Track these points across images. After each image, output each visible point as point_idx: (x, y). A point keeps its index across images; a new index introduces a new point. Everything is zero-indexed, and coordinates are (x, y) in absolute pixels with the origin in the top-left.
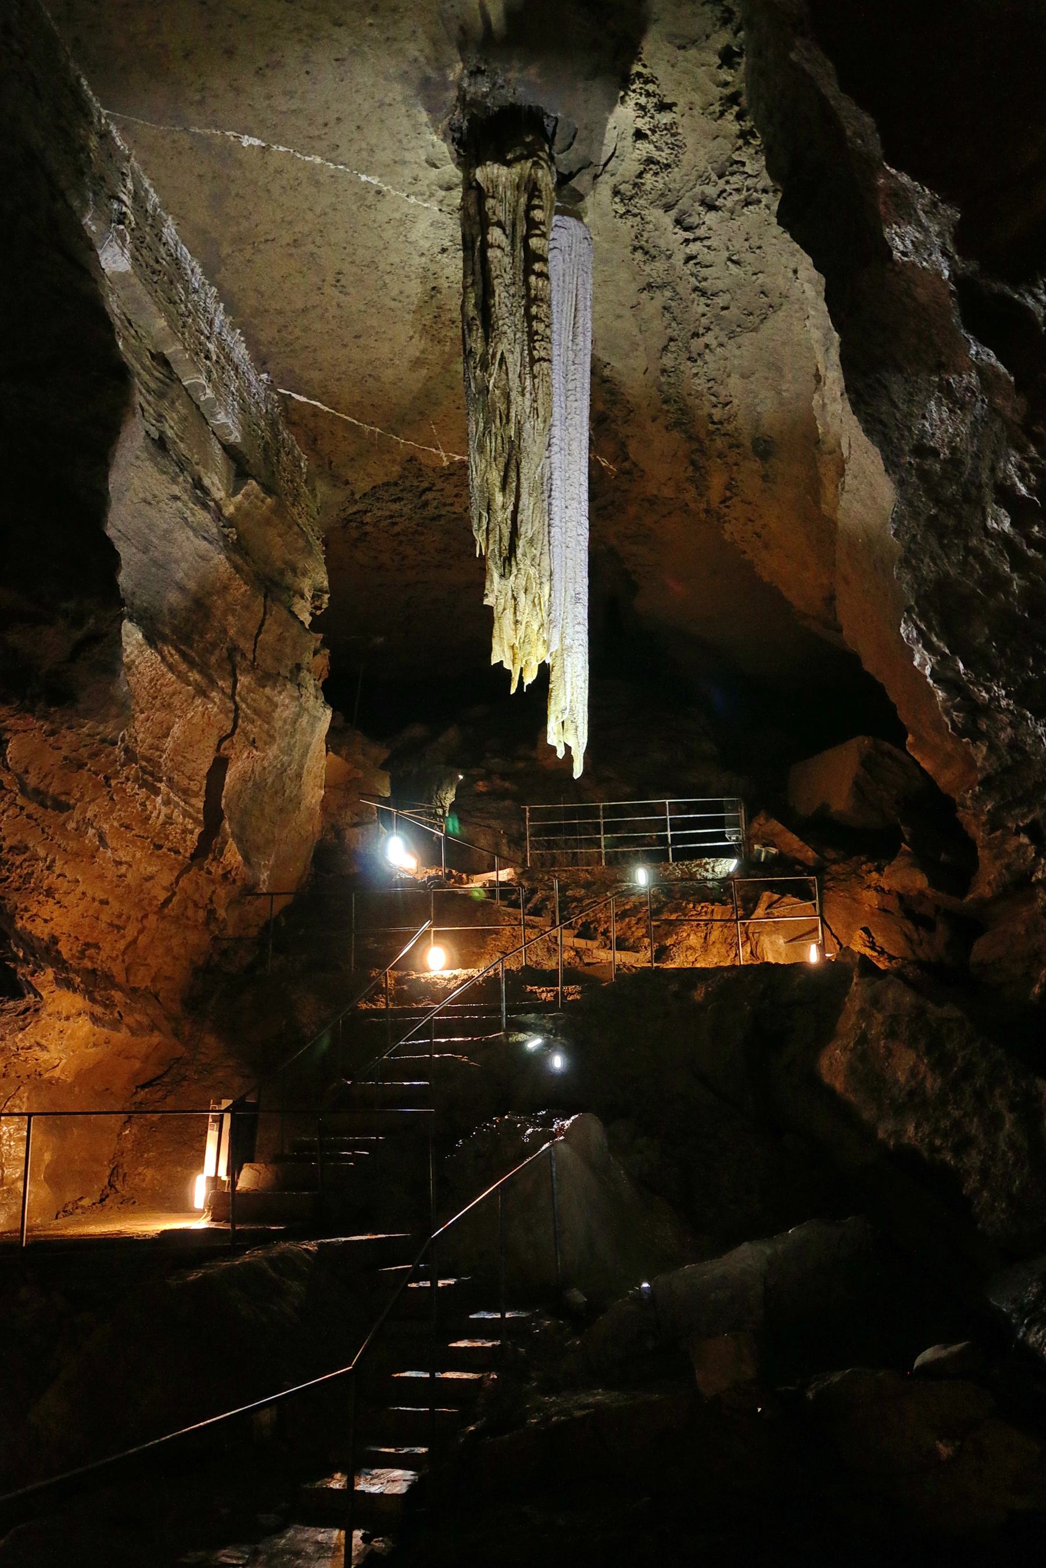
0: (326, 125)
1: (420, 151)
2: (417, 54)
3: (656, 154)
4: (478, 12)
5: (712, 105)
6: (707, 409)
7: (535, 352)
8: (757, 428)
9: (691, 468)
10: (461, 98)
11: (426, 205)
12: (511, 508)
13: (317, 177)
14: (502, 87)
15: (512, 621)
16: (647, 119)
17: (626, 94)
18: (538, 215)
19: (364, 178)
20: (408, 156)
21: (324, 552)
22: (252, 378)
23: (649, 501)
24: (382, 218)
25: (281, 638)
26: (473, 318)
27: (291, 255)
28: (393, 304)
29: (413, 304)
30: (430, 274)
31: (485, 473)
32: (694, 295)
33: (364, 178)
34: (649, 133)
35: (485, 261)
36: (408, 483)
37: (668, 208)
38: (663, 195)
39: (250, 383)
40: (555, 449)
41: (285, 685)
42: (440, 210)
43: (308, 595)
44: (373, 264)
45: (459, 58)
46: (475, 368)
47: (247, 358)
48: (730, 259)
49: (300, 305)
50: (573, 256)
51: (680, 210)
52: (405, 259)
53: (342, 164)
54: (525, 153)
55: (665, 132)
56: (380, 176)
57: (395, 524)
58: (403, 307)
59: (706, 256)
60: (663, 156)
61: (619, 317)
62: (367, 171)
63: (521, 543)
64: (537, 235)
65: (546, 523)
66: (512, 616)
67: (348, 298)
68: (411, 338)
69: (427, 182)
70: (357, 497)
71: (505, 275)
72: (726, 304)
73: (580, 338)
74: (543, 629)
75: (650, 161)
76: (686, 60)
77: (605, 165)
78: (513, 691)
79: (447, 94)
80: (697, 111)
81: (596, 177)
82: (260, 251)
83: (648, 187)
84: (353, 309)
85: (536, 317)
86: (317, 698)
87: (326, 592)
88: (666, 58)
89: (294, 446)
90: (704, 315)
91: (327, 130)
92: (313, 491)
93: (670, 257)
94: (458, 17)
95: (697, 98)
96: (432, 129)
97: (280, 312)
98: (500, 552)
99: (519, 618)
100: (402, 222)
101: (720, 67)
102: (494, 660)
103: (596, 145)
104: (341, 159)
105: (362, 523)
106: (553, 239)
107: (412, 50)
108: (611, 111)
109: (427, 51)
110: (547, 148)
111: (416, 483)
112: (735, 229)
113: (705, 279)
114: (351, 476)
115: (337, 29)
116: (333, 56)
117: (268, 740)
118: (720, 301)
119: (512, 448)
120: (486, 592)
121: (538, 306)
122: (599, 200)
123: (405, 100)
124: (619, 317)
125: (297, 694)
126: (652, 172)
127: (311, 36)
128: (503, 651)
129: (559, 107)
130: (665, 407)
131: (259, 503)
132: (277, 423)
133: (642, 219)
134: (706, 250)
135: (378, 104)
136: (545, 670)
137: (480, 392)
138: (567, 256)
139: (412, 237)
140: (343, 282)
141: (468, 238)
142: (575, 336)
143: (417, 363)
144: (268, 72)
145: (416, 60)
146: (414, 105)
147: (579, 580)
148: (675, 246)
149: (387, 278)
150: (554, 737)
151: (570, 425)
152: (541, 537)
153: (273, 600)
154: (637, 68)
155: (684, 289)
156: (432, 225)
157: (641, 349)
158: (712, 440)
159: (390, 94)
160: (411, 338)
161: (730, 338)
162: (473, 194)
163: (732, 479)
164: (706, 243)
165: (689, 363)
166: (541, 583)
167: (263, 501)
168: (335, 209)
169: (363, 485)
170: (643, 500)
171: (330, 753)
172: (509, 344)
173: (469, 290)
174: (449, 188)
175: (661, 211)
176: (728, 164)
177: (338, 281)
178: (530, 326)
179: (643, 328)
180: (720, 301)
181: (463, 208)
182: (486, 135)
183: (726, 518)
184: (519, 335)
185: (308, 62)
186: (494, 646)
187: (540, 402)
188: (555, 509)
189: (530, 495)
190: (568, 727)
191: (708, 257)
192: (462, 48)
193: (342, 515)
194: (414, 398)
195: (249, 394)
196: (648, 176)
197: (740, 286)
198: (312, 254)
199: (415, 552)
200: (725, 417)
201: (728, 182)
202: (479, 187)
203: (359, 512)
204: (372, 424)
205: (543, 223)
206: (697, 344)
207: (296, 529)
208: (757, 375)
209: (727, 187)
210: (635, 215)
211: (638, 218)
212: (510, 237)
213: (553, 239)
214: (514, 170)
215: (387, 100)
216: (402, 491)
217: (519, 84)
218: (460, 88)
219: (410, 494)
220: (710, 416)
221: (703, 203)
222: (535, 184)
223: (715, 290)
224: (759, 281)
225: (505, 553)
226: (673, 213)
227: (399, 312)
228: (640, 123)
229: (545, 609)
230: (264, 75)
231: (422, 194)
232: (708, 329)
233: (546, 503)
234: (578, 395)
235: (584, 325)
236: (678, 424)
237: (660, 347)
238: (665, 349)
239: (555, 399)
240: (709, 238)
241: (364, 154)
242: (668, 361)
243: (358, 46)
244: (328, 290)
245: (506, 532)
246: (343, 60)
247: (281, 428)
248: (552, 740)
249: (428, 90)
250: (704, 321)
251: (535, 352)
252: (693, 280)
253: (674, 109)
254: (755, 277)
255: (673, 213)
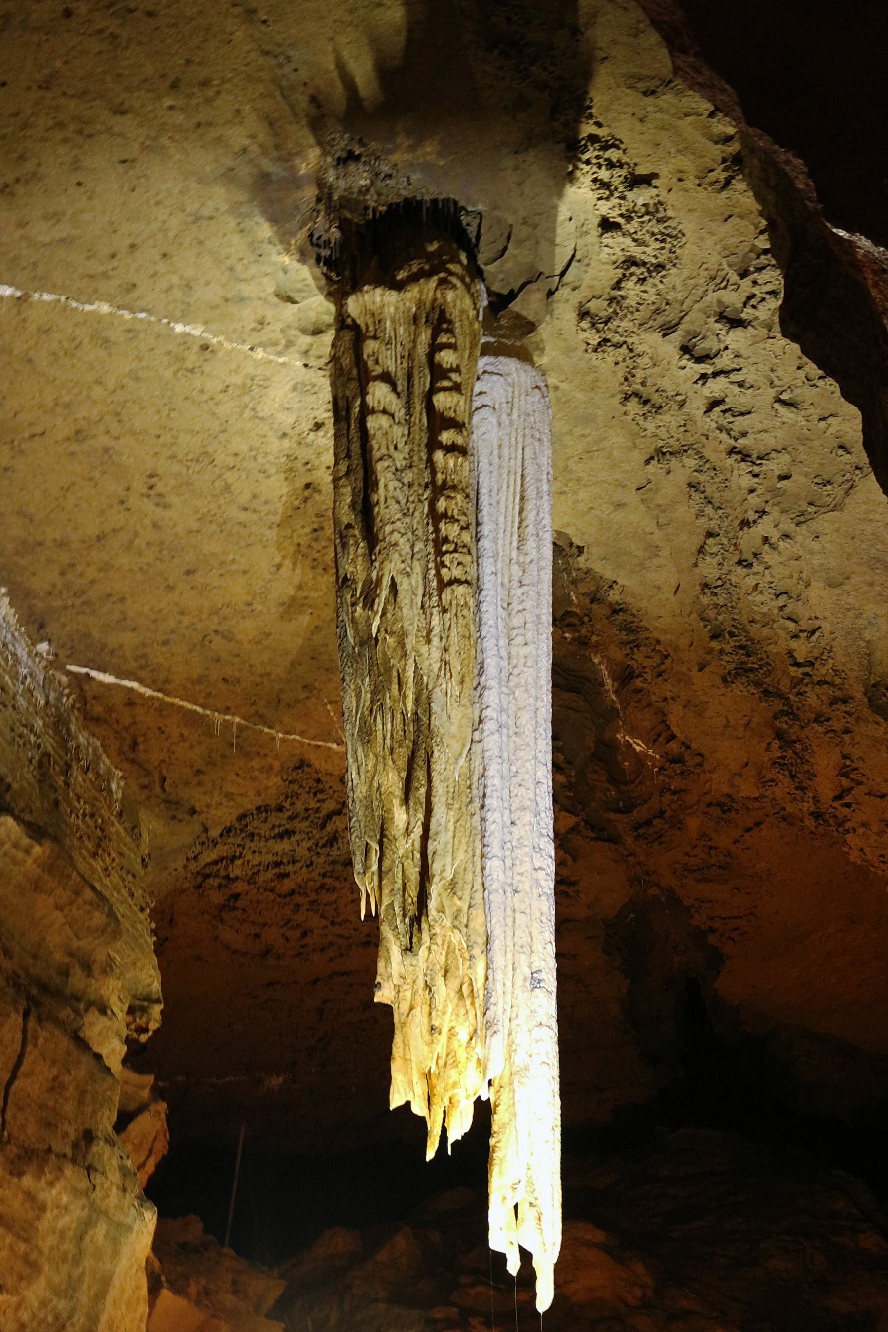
0: (113, 256)
1: (265, 281)
2: (247, 142)
3: (637, 252)
4: (335, 74)
5: (712, 171)
6: (784, 644)
7: (444, 571)
8: (870, 668)
9: (776, 744)
10: (325, 194)
11: (281, 360)
12: (418, 831)
13: (105, 334)
14: (390, 176)
15: (425, 1028)
16: (614, 201)
17: (576, 167)
18: (447, 358)
19: (179, 328)
20: (246, 290)
21: (154, 932)
22: (22, 652)
23: (719, 804)
24: (213, 386)
25: (56, 1086)
26: (349, 526)
27: (73, 454)
28: (243, 516)
29: (275, 513)
30: (299, 464)
31: (371, 774)
32: (731, 461)
33: (179, 328)
34: (620, 220)
35: (364, 435)
36: (299, 806)
37: (667, 330)
38: (657, 311)
39: (17, 661)
40: (489, 726)
41: (60, 1169)
42: (306, 365)
43: (119, 1009)
44: (205, 457)
45: (312, 140)
46: (354, 604)
47: (13, 620)
48: (778, 400)
49: (93, 530)
50: (515, 416)
51: (688, 332)
52: (258, 445)
53: (142, 311)
54: (427, 267)
55: (646, 218)
56: (206, 323)
57: (286, 875)
58: (260, 519)
59: (737, 398)
60: (649, 253)
61: (619, 505)
62: (184, 318)
63: (435, 890)
64: (445, 389)
65: (478, 853)
66: (425, 1021)
67: (168, 513)
68: (279, 567)
69: (279, 326)
70: (214, 833)
71: (396, 455)
72: (785, 472)
73: (531, 544)
74: (483, 1040)
75: (631, 262)
76: (660, 110)
77: (563, 274)
78: (430, 1155)
79: (300, 194)
80: (690, 182)
81: (550, 293)
82: (22, 452)
83: (632, 301)
84: (180, 529)
85: (445, 515)
86: (124, 1190)
87: (158, 1001)
88: (629, 110)
89: (98, 757)
90: (752, 491)
91: (115, 263)
92: (134, 830)
93: (682, 404)
94: (305, 84)
95: (686, 163)
96: (280, 247)
97: (62, 544)
98: (404, 909)
99: (436, 1023)
100: (246, 389)
101: (712, 115)
102: (396, 1101)
103: (544, 246)
104: (139, 303)
105: (227, 877)
106: (481, 393)
107: (238, 137)
108: (560, 194)
109: (261, 136)
110: (463, 257)
111: (313, 804)
112: (779, 352)
113: (744, 434)
114: (199, 799)
115: (119, 119)
116: (115, 158)
117: (27, 1271)
118: (774, 466)
119: (418, 731)
120: (379, 979)
121: (449, 497)
122: (560, 330)
123: (234, 209)
124: (619, 505)
125: (84, 1184)
126: (634, 278)
127: (80, 132)
128: (411, 1083)
129: (482, 194)
130: (714, 644)
131: (20, 855)
132: (67, 723)
133: (631, 350)
134: (736, 389)
135: (190, 219)
136: (483, 1111)
137: (362, 644)
138: (504, 417)
139: (265, 410)
140: (160, 488)
141: (342, 404)
142: (521, 540)
143: (292, 607)
144: (20, 190)
145: (244, 150)
146: (247, 215)
147: (538, 947)
148: (687, 388)
149: (231, 477)
150: (502, 1237)
151: (517, 686)
152: (469, 877)
153: (40, 1020)
154: (587, 129)
155: (715, 452)
156: (294, 388)
157: (665, 553)
158: (799, 693)
159: (209, 203)
160: (279, 567)
161: (798, 524)
162: (348, 336)
163: (845, 757)
164: (736, 377)
165: (739, 570)
166: (472, 957)
167: (27, 852)
168: (137, 379)
169: (224, 815)
170: (710, 805)
171: (166, 1294)
172: (403, 565)
173: (341, 483)
174: (317, 332)
175: (657, 337)
176: (753, 255)
177: (151, 488)
178: (437, 530)
179: (662, 521)
180: (774, 466)
181: (334, 359)
182: (364, 248)
183: (848, 825)
184: (419, 546)
185: (77, 169)
186: (394, 1074)
187: (452, 650)
188: (491, 828)
189: (449, 806)
190: (527, 1214)
191: (742, 399)
192: (317, 124)
193: (193, 866)
194: (292, 664)
195: (15, 677)
196: (629, 284)
197: (803, 440)
198: (106, 450)
199: (324, 922)
200: (816, 653)
201: (755, 283)
202: (355, 327)
203: (222, 859)
204: (227, 710)
205: (457, 370)
206: (750, 539)
207: (88, 894)
208: (855, 579)
209: (756, 290)
210: (618, 346)
211: (624, 350)
212: (404, 395)
213: (481, 393)
214: (408, 295)
215: (206, 212)
216: (291, 819)
217: (410, 170)
218: (320, 183)
219: (307, 824)
220: (790, 653)
221: (721, 317)
222: (442, 312)
223: (763, 450)
224: (831, 430)
225: (412, 910)
226: (677, 337)
227: (254, 529)
228: (604, 208)
229: (479, 1002)
230: (12, 194)
231: (275, 344)
232: (762, 513)
233: (477, 818)
234: (529, 635)
235: (537, 523)
236: (742, 671)
237: (694, 549)
238: (701, 550)
239: (489, 644)
240: (740, 369)
241: (177, 293)
242: (709, 569)
243: (155, 139)
244: (134, 501)
245: (414, 874)
246: (134, 160)
247: (73, 728)
248: (496, 1242)
249: (268, 193)
250: (754, 500)
251: (444, 571)
252: (724, 436)
253: (655, 182)
254: (823, 424)
255: (677, 337)
